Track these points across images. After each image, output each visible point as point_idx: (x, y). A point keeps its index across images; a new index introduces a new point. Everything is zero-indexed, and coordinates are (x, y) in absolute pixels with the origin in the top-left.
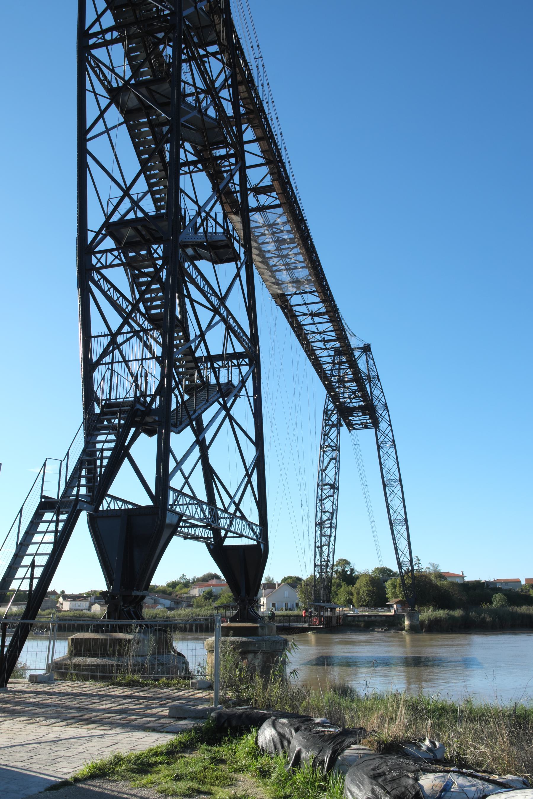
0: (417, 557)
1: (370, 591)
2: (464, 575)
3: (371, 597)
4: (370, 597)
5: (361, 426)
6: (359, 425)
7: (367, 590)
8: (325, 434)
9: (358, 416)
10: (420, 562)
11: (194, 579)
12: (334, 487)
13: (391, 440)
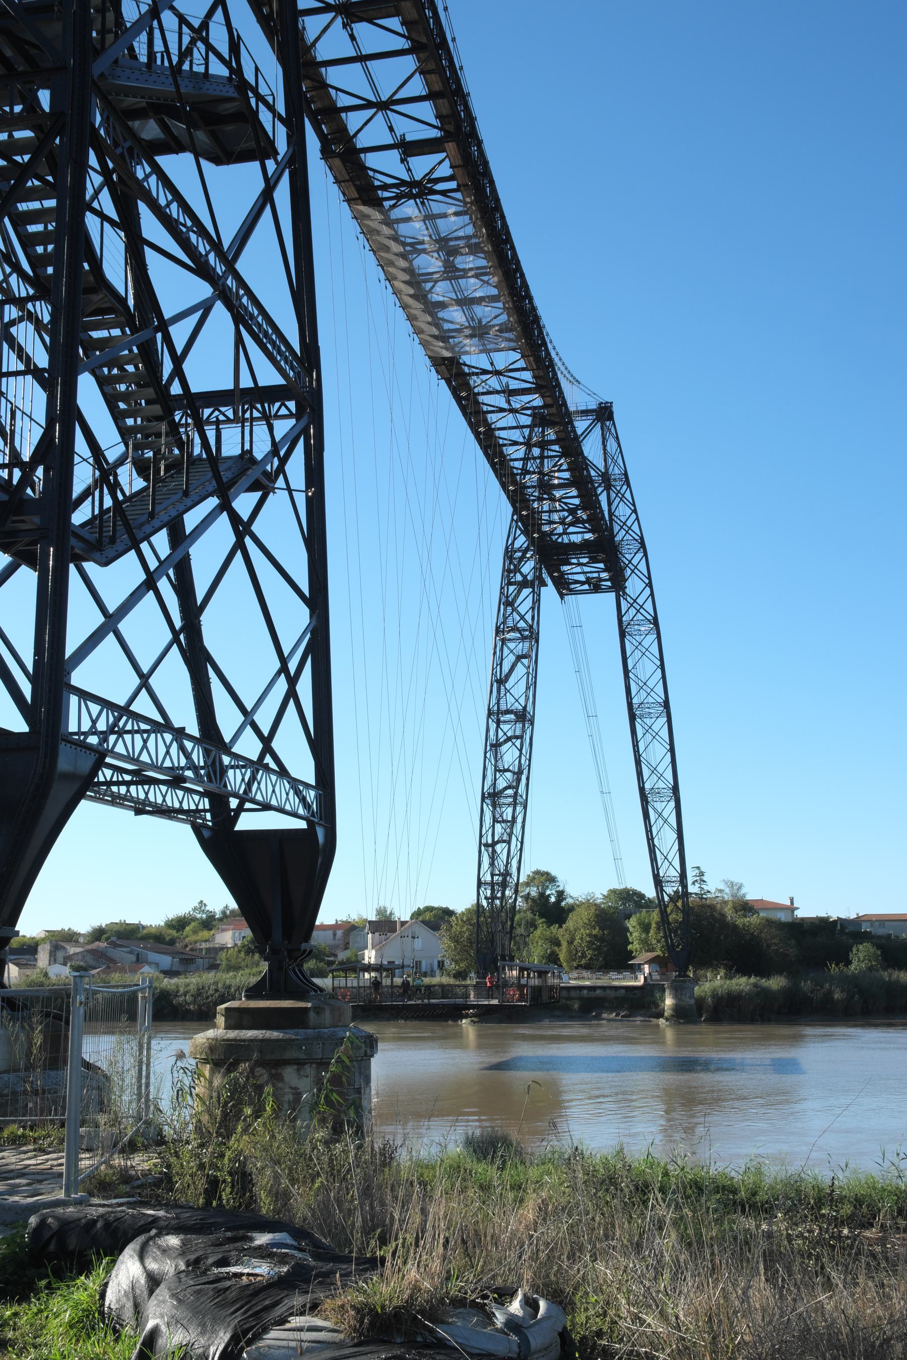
0: (698, 868)
1: (595, 936)
2: (795, 905)
3: (598, 949)
4: (594, 950)
5: (586, 587)
6: (583, 583)
7: (590, 935)
8: (508, 603)
9: (579, 564)
10: (704, 878)
11: (224, 912)
12: (524, 717)
13: (649, 617)
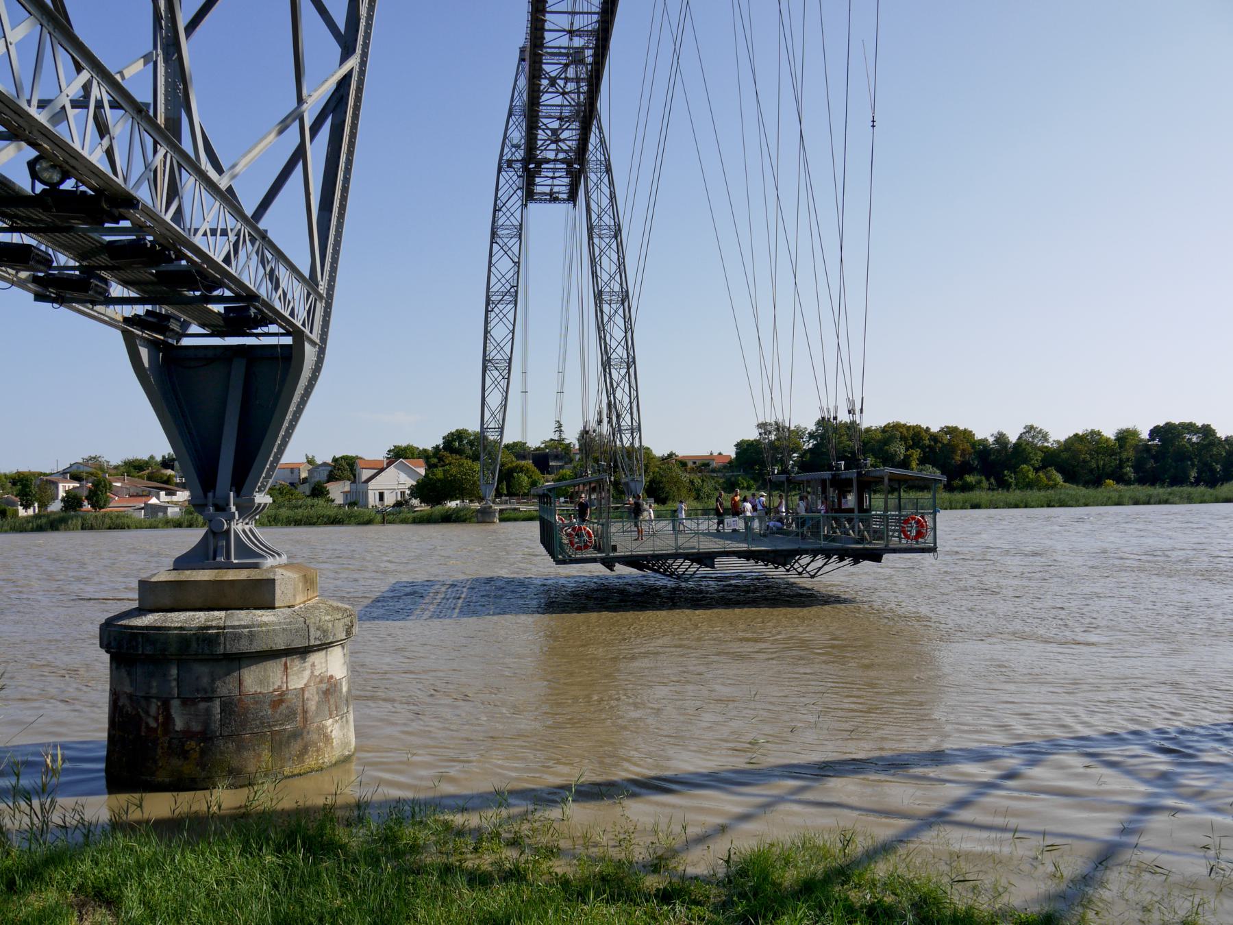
13: (516, 223)
